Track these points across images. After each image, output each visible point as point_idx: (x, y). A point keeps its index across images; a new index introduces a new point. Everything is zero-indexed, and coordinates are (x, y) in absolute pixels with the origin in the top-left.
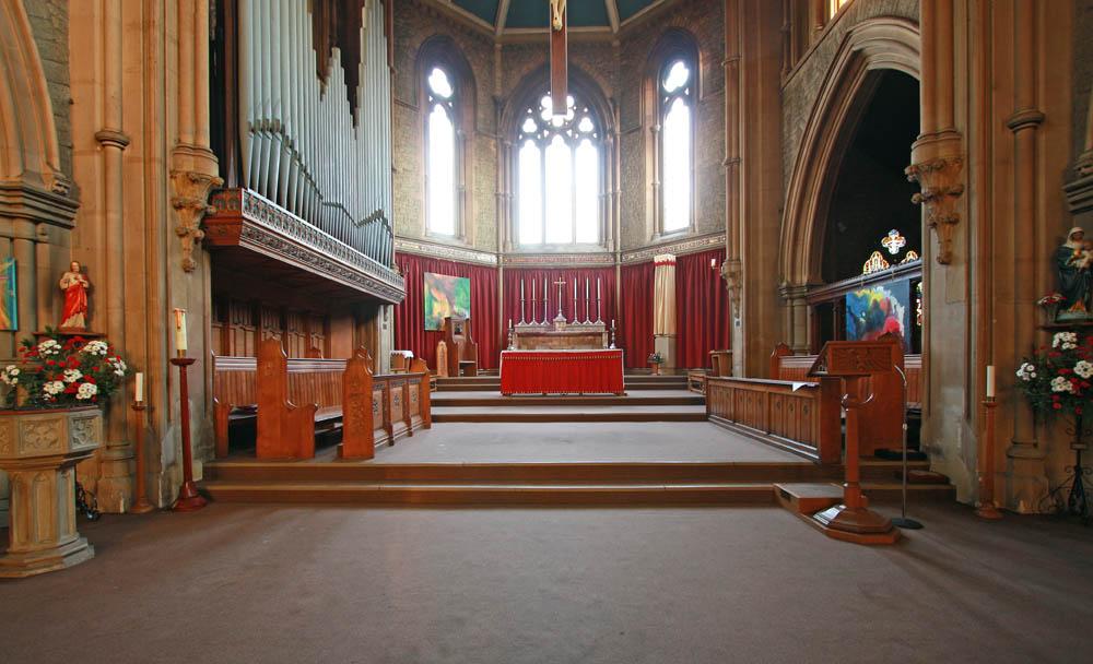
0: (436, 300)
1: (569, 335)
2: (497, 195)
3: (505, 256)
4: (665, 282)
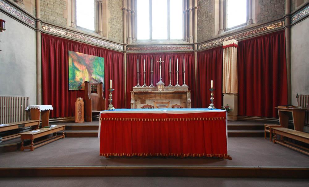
0: (78, 70)
1: (166, 93)
2: (123, 9)
3: (128, 46)
4: (230, 59)
